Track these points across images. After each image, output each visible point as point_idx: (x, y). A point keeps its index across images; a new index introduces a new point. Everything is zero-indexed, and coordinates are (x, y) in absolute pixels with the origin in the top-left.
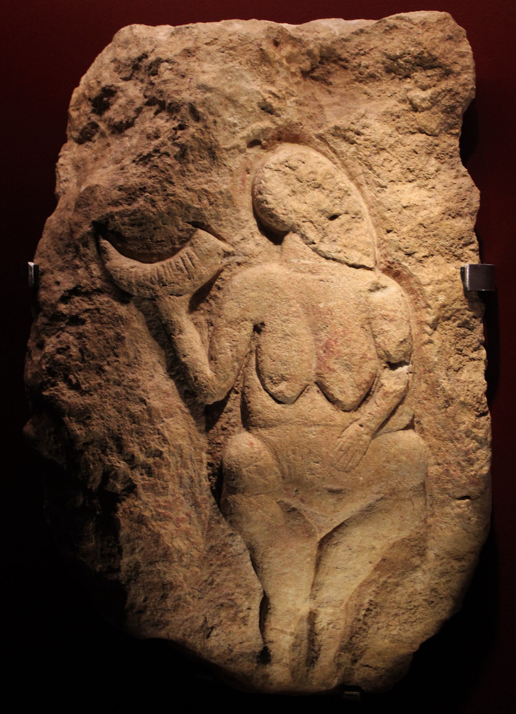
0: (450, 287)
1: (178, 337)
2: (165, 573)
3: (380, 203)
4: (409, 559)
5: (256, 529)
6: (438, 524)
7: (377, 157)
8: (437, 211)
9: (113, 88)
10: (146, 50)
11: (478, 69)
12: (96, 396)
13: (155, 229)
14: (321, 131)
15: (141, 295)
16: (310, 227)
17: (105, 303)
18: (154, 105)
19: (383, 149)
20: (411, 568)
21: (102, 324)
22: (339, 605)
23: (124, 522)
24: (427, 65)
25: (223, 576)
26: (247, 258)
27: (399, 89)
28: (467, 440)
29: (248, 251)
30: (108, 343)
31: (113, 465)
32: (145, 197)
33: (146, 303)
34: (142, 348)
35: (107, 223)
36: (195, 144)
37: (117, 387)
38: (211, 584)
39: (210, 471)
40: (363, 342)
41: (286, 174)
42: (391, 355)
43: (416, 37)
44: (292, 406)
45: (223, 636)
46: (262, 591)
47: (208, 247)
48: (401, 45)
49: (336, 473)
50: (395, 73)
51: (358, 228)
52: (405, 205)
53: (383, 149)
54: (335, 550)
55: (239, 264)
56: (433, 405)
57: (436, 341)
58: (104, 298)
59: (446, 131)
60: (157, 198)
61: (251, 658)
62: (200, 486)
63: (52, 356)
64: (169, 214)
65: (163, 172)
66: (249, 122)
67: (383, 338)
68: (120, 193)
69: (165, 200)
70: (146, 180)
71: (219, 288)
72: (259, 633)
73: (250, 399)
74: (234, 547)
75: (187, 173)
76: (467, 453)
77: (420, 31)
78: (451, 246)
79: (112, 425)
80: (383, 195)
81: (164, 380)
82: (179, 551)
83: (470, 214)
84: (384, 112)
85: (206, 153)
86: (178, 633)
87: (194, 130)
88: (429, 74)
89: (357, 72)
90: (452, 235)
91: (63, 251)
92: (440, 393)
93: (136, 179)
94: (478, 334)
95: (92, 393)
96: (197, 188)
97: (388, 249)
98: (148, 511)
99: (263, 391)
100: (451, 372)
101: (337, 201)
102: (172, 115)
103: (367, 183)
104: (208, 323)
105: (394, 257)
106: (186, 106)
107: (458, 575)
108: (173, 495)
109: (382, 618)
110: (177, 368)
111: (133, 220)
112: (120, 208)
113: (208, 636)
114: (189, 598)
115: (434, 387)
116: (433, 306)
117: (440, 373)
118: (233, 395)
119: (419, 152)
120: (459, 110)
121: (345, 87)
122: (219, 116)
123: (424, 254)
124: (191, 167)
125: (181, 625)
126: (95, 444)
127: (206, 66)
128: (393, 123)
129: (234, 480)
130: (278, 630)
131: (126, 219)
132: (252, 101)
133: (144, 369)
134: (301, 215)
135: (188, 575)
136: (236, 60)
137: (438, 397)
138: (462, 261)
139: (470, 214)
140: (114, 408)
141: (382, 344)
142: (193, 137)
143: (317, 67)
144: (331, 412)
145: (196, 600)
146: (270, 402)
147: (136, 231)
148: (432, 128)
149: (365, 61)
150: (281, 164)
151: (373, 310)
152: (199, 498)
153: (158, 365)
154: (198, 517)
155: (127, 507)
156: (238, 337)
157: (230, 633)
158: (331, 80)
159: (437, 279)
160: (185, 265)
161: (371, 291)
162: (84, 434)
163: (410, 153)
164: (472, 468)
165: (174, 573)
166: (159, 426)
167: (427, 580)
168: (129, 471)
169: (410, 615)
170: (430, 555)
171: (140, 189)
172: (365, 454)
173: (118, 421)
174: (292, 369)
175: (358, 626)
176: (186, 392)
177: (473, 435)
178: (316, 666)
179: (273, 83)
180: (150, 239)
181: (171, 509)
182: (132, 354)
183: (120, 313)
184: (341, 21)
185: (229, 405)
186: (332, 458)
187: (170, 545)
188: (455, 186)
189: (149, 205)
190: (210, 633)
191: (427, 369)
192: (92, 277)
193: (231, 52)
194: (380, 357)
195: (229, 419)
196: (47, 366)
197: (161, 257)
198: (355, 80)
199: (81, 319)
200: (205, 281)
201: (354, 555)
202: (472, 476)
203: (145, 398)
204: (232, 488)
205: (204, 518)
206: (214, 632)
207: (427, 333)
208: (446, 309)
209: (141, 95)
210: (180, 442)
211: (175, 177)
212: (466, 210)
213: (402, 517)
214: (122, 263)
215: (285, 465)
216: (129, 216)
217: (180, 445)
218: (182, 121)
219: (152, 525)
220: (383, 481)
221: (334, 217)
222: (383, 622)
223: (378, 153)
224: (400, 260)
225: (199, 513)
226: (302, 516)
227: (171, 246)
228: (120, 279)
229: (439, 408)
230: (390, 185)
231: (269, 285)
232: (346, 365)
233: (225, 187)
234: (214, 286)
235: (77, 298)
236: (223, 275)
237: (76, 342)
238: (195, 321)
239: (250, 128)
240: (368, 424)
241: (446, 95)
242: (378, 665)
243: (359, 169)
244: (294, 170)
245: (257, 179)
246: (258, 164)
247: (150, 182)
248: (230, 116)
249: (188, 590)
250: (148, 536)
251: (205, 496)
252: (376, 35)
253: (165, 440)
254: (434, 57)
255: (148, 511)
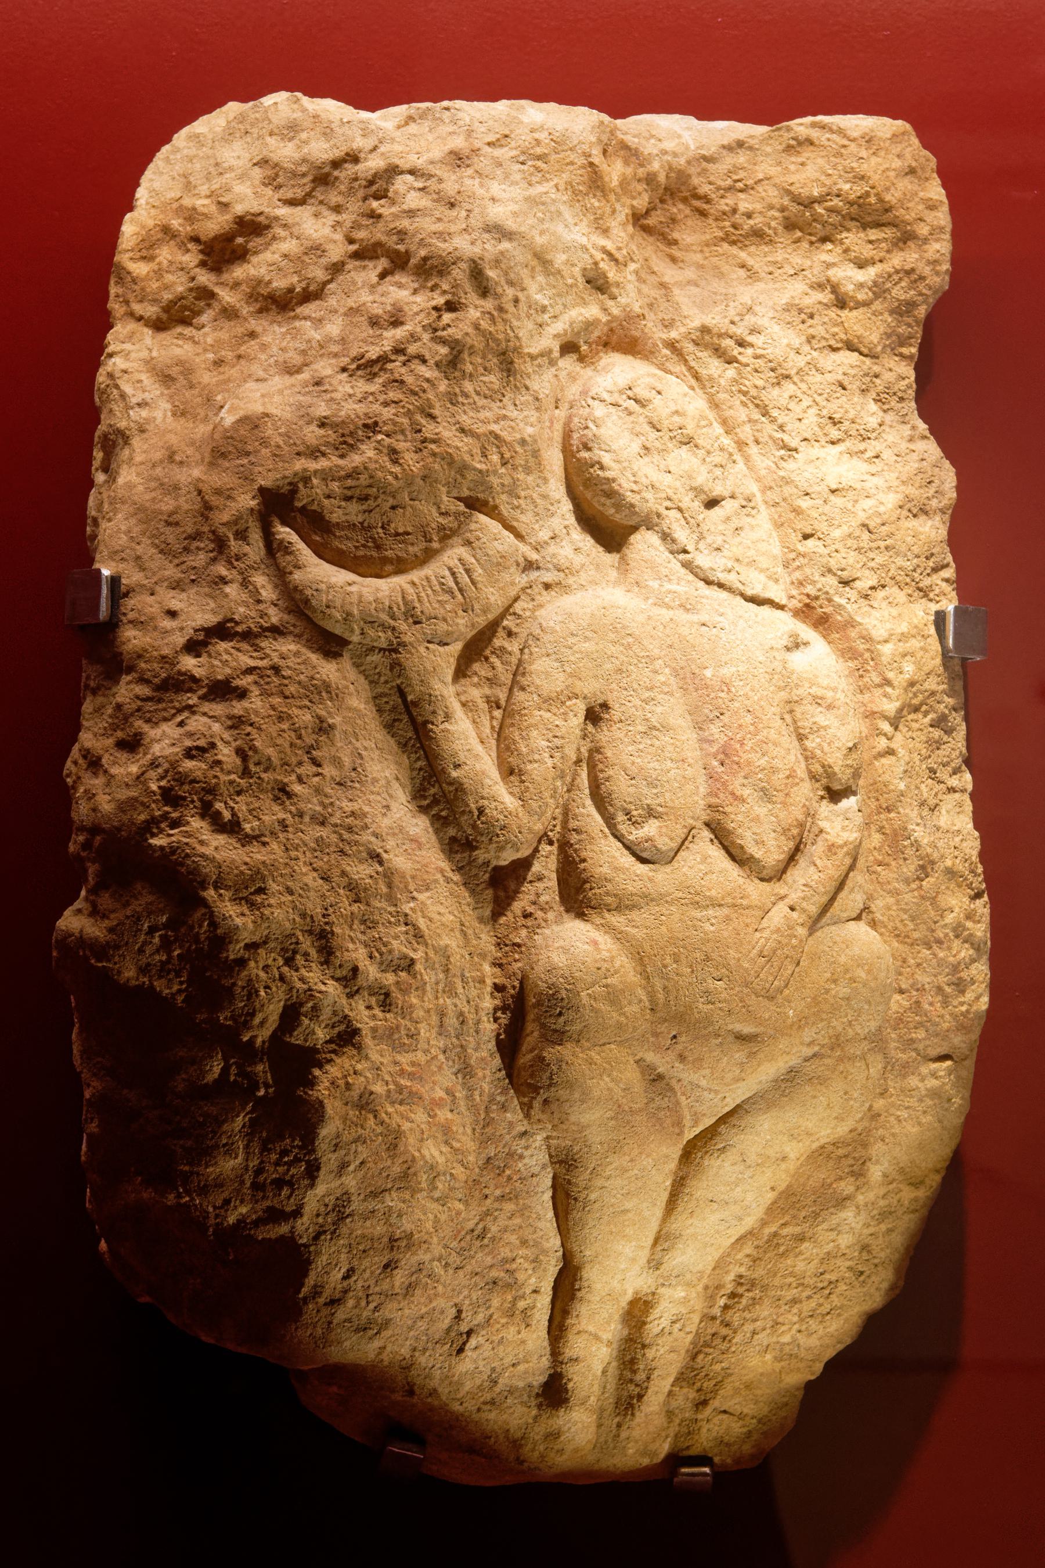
0: (922, 648)
1: (442, 727)
2: (400, 1216)
3: (787, 481)
4: (830, 1185)
5: (591, 1119)
6: (892, 1110)
7: (776, 392)
8: (891, 500)
9: (261, 219)
10: (355, 146)
11: (955, 235)
12: (274, 846)
13: (393, 508)
14: (674, 334)
15: (367, 641)
16: (678, 520)
17: (291, 655)
18: (374, 257)
19: (788, 377)
20: (833, 1203)
21: (286, 697)
22: (696, 1282)
23: (333, 1107)
24: (869, 219)
25: (502, 1222)
26: (562, 574)
27: (808, 263)
28: (956, 944)
29: (563, 563)
30: (300, 737)
31: (310, 990)
32: (379, 442)
33: (375, 658)
34: (366, 749)
35: (294, 491)
36: (478, 343)
37: (318, 828)
38: (481, 1237)
39: (497, 1002)
40: (787, 746)
41: (630, 414)
42: (835, 774)
43: (854, 165)
44: (668, 869)
45: (486, 1351)
46: (560, 1253)
47: (500, 548)
48: (823, 178)
49: (752, 1000)
50: (801, 230)
51: (752, 527)
52: (834, 487)
53: (788, 377)
54: (719, 1162)
55: (547, 586)
56: (895, 876)
57: (901, 752)
58: (288, 646)
59: (892, 349)
60: (401, 446)
61: (525, 1398)
62: (477, 1032)
63: (174, 765)
64: (424, 478)
65: (414, 393)
66: (565, 306)
67: (818, 740)
68: (322, 432)
69: (418, 451)
70: (376, 407)
71: (510, 634)
72: (546, 1343)
73: (583, 854)
74: (526, 1161)
75: (460, 399)
76: (955, 968)
77: (864, 153)
78: (914, 570)
79: (310, 905)
80: (791, 465)
81: (409, 815)
82: (432, 1168)
83: (941, 510)
84: (787, 304)
85: (495, 360)
86: (402, 1346)
87: (478, 314)
88: (873, 238)
89: (727, 224)
90: (916, 550)
91: (178, 547)
92: (910, 852)
93: (356, 406)
94: (957, 744)
95: (266, 839)
96: (481, 429)
97: (808, 571)
98: (380, 1083)
99: (611, 838)
100: (925, 812)
101: (718, 472)
102: (426, 280)
103: (757, 442)
104: (488, 702)
105: (819, 586)
106: (464, 265)
107: (906, 1217)
108: (426, 1052)
109: (765, 1311)
110: (432, 791)
111: (349, 488)
112: (323, 463)
113: (461, 1350)
114: (438, 1268)
115: (897, 840)
116: (896, 683)
117: (910, 812)
118: (545, 848)
119: (849, 387)
120: (922, 311)
121: (701, 251)
122: (523, 290)
123: (870, 583)
124: (468, 386)
125: (410, 1328)
126: (272, 945)
127: (496, 188)
128: (801, 326)
129: (560, 1014)
130: (591, 1334)
131: (335, 486)
132: (573, 265)
133: (372, 793)
134: (664, 495)
135: (443, 1217)
136: (547, 180)
137: (905, 859)
138: (931, 600)
139: (941, 510)
140: (315, 870)
141: (818, 752)
142: (477, 327)
143: (654, 209)
144: (741, 881)
145: (451, 1271)
146: (627, 860)
147: (353, 512)
148: (871, 342)
149: (744, 203)
150: (621, 392)
151: (797, 686)
152: (474, 1056)
153: (396, 785)
154: (467, 1097)
155: (340, 1076)
156: (563, 730)
157: (501, 1341)
158: (676, 235)
159: (899, 631)
160: (457, 583)
161: (788, 649)
162: (251, 926)
163: (834, 387)
164: (962, 999)
165: (418, 1214)
166: (407, 907)
167: (859, 1226)
168: (344, 1001)
169: (821, 1300)
170: (875, 1173)
171: (365, 426)
172: (798, 964)
173: (323, 896)
174: (667, 795)
175: (710, 1331)
176: (453, 840)
177: (966, 933)
178: (637, 1414)
179: (605, 232)
180: (383, 527)
181: (421, 1079)
182: (347, 761)
183: (325, 677)
184: (691, 120)
185: (536, 867)
186: (746, 970)
187: (417, 1154)
188: (915, 456)
189: (386, 459)
190: (464, 1344)
191: (884, 806)
192: (259, 602)
193: (539, 163)
194: (813, 777)
195: (538, 895)
196: (163, 783)
197: (401, 566)
198: (723, 239)
199: (237, 688)
200: (491, 617)
201: (748, 1173)
202: (962, 1014)
203: (380, 851)
204: (555, 1031)
205: (478, 1098)
206: (473, 1342)
207: (885, 735)
208: (914, 689)
209: (339, 237)
210: (445, 941)
211: (437, 405)
212: (934, 503)
213: (846, 1093)
214: (318, 573)
215: (658, 984)
216: (340, 479)
217: (447, 946)
218: (454, 294)
219: (386, 1113)
220: (822, 1020)
221: (711, 503)
222: (765, 1319)
223: (778, 384)
224: (832, 592)
225: (471, 1089)
226: (672, 1089)
227: (423, 545)
228: (328, 607)
229: (907, 881)
230: (803, 447)
231: (609, 628)
232: (763, 789)
233: (530, 430)
234: (500, 629)
235: (223, 646)
236: (518, 607)
237: (226, 736)
238: (463, 698)
239: (566, 317)
240: (804, 904)
241: (900, 279)
242: (746, 1411)
243: (741, 414)
244: (643, 406)
245: (576, 420)
246: (573, 391)
247: (387, 413)
248: (537, 290)
249: (437, 1250)
250: (377, 1136)
251: (484, 1054)
252: (767, 155)
253: (419, 936)
254: (887, 206)
255: (380, 1083)
